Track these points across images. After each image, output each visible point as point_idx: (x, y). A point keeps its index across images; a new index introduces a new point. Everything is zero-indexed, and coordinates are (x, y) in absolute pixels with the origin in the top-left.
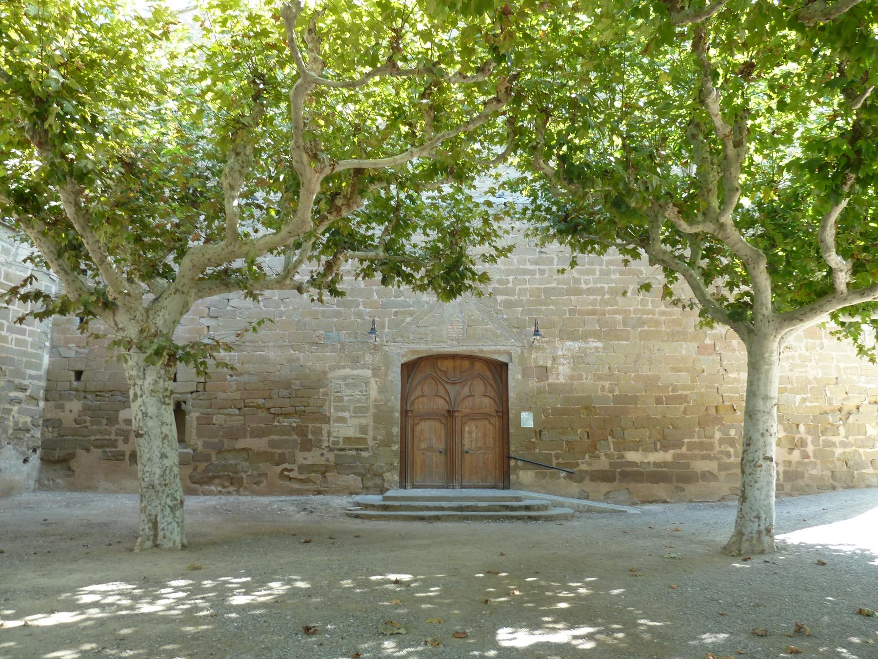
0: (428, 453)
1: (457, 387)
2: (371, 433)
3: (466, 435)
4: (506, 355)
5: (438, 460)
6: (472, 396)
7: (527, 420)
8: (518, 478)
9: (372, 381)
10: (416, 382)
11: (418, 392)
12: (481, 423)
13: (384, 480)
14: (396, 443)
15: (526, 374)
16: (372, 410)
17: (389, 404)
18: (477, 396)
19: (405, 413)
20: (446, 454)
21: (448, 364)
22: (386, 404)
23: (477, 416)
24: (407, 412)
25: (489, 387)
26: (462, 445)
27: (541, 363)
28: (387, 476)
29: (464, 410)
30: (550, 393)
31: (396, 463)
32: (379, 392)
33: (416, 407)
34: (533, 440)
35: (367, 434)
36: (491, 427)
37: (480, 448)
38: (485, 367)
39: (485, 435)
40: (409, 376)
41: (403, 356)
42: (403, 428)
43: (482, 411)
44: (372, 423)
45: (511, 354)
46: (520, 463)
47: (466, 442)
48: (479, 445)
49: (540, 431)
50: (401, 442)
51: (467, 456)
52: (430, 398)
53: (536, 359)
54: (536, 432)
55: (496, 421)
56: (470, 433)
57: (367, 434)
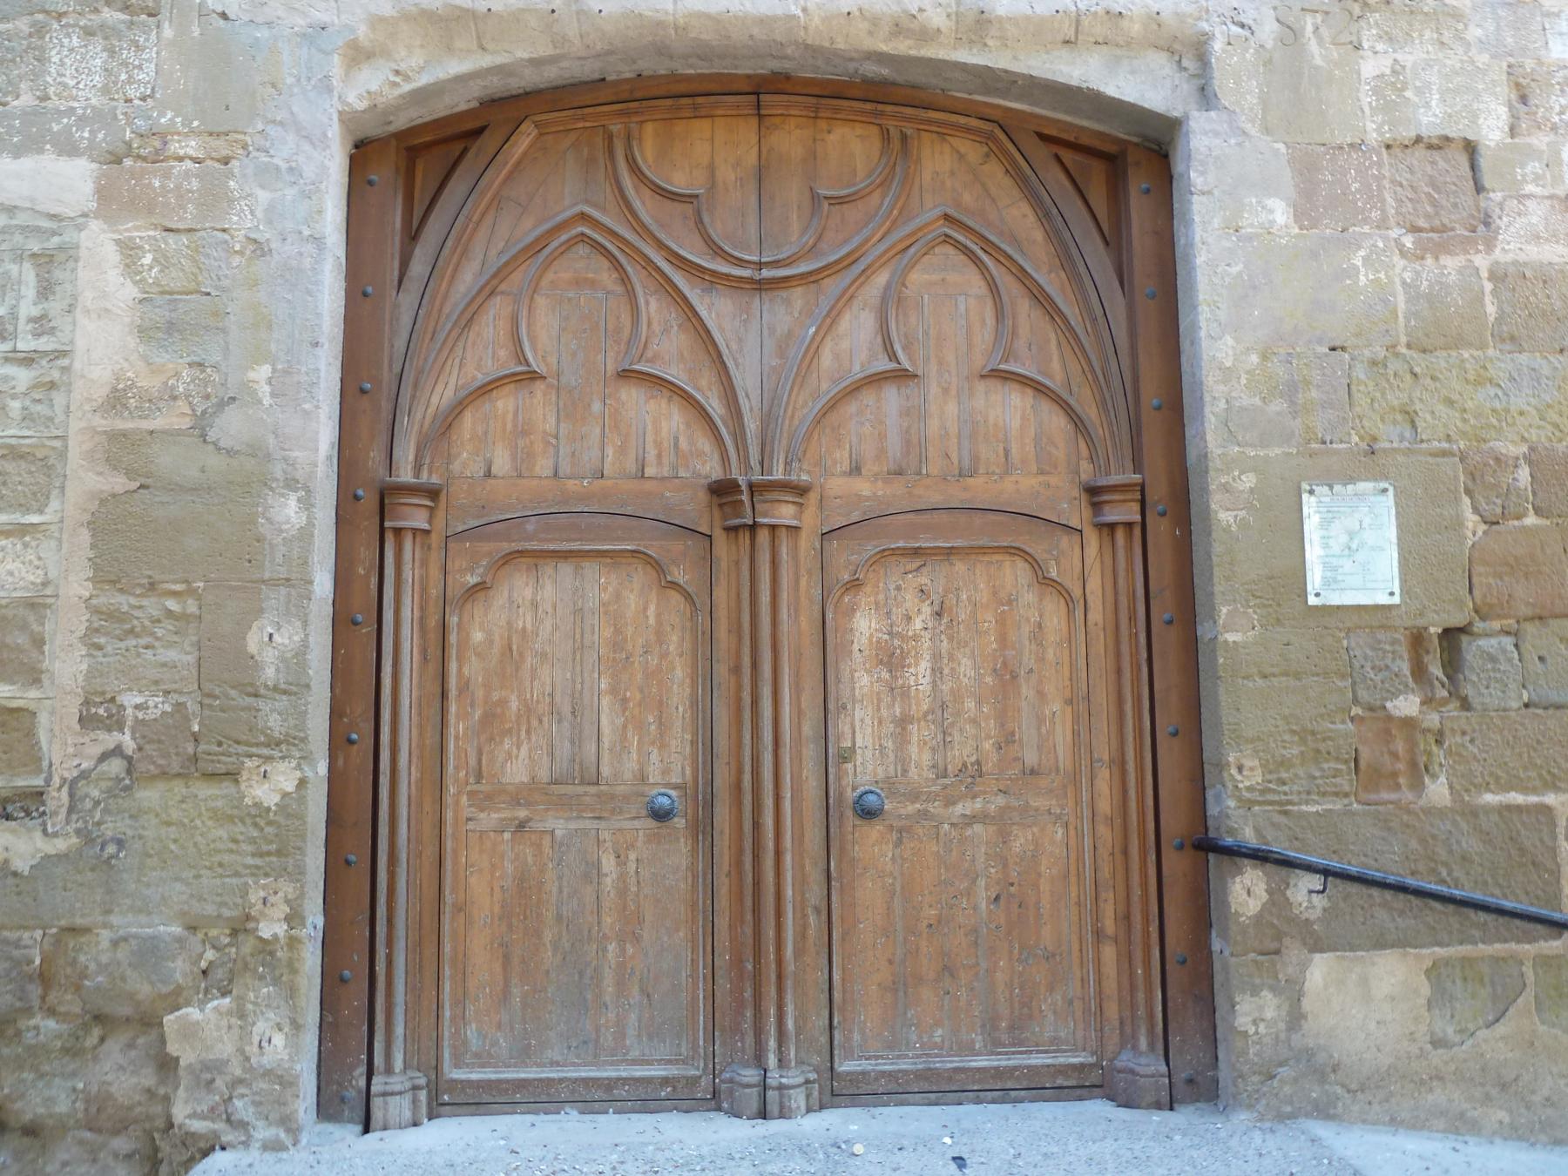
0: (560, 826)
1: (784, 314)
2: (68, 667)
3: (861, 679)
4: (1160, 63)
5: (639, 875)
6: (902, 376)
7: (1354, 552)
8: (1296, 1018)
9: (98, 244)
10: (468, 279)
11: (485, 352)
12: (975, 585)
13: (167, 1065)
14: (287, 744)
15: (1319, 184)
16: (86, 480)
17: (231, 426)
18: (933, 372)
19: (374, 508)
20: (702, 828)
21: (709, 154)
22: (201, 428)
23: (936, 531)
24: (387, 497)
25: (1026, 313)
26: (831, 757)
27: (1430, 118)
28: (200, 1028)
29: (837, 485)
30: (1514, 341)
31: (292, 913)
32: (144, 332)
33: (465, 461)
34: (1407, 705)
35: (34, 676)
36: (1055, 618)
37: (973, 774)
38: (995, 172)
39: (1007, 677)
40: (412, 235)
41: (358, 55)
42: (358, 626)
43: (980, 489)
44: (77, 586)
45: (1200, 50)
46: (1303, 891)
47: (864, 733)
48: (961, 752)
49: (1451, 635)
50: (339, 742)
51: (871, 845)
52: (570, 390)
53: (1394, 84)
54: (1417, 640)
55: (1087, 564)
56: (891, 659)
57: (34, 676)
